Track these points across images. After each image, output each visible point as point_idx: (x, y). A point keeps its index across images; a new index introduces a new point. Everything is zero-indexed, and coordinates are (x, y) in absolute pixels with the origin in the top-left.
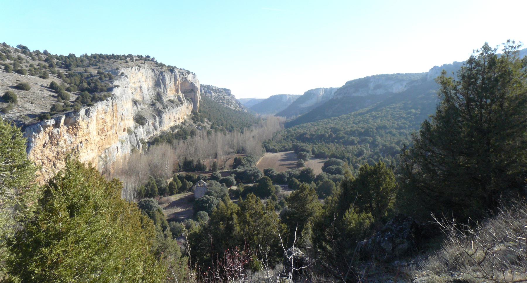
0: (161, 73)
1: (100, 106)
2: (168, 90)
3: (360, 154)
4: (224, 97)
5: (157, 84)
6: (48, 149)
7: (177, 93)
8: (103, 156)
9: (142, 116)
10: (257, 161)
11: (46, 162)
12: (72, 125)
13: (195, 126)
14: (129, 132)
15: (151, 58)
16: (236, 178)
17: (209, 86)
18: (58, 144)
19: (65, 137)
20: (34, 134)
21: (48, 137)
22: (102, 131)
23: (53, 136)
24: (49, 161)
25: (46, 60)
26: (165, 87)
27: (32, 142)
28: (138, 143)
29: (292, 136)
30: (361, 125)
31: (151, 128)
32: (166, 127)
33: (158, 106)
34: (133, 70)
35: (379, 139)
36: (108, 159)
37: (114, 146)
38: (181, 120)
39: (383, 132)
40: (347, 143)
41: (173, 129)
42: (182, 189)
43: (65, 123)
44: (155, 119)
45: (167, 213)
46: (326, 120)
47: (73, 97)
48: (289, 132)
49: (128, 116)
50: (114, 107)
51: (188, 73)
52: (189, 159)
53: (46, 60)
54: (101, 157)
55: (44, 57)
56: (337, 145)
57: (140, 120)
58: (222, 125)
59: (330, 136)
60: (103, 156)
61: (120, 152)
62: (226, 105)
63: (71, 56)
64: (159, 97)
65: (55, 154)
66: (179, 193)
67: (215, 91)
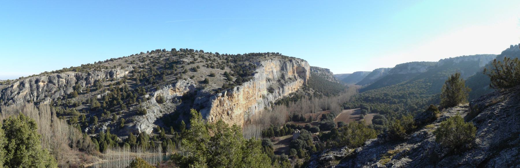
0: (285, 62)
1: (246, 84)
3: (397, 110)
5: (282, 69)
10: (337, 115)
13: (304, 93)
14: (264, 97)
16: (320, 128)
22: (247, 98)
24: (220, 114)
25: (226, 59)
28: (268, 104)
29: (361, 98)
30: (401, 92)
31: (277, 94)
32: (286, 94)
33: (282, 81)
35: (409, 100)
37: (254, 106)
38: (296, 90)
39: (412, 96)
40: (391, 103)
41: (290, 95)
42: (287, 134)
43: (227, 95)
45: (275, 148)
46: (382, 88)
47: (234, 79)
48: (360, 95)
51: (302, 60)
52: (297, 113)
53: (226, 59)
55: (225, 57)
56: (386, 104)
57: (271, 90)
58: (321, 92)
59: (383, 98)
61: (257, 109)
62: (326, 79)
63: (239, 55)
64: (283, 77)
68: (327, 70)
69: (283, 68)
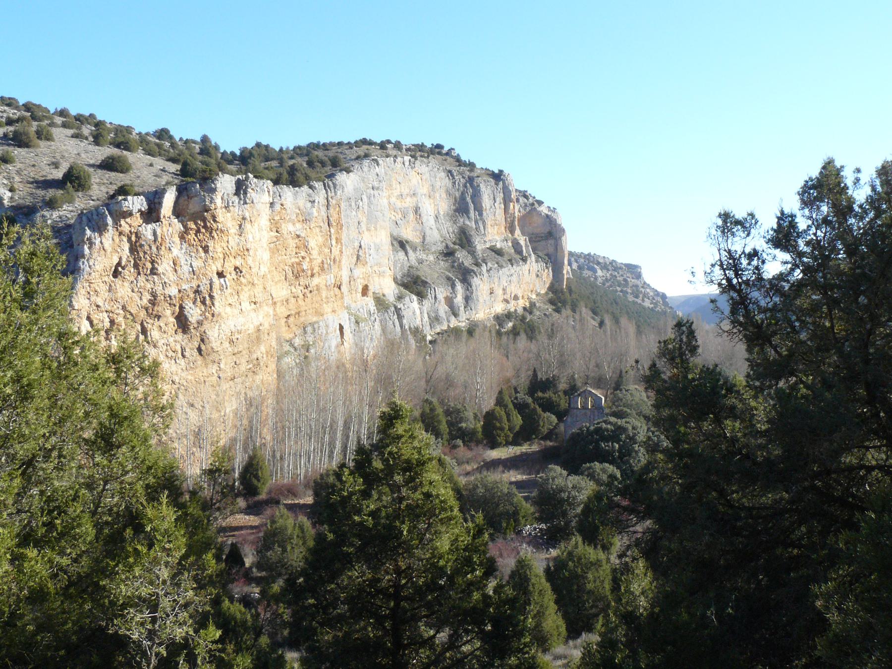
0: (471, 180)
2: (489, 223)
4: (625, 280)
5: (461, 208)
6: (126, 284)
7: (512, 232)
8: (297, 342)
9: (418, 277)
11: (120, 320)
12: (195, 217)
15: (446, 149)
17: (589, 255)
18: (154, 271)
19: (176, 251)
20: (88, 232)
21: (126, 246)
23: (141, 246)
26: (481, 214)
27: (83, 256)
31: (443, 309)
33: (461, 258)
34: (399, 165)
36: (312, 351)
37: (333, 322)
38: (522, 303)
43: (177, 212)
44: (453, 286)
49: (379, 264)
50: (332, 210)
54: (292, 345)
57: (414, 284)
60: (297, 342)
62: (631, 298)
65: (145, 301)
66: (515, 443)
67: (604, 267)
68: (633, 270)
69: (465, 203)
